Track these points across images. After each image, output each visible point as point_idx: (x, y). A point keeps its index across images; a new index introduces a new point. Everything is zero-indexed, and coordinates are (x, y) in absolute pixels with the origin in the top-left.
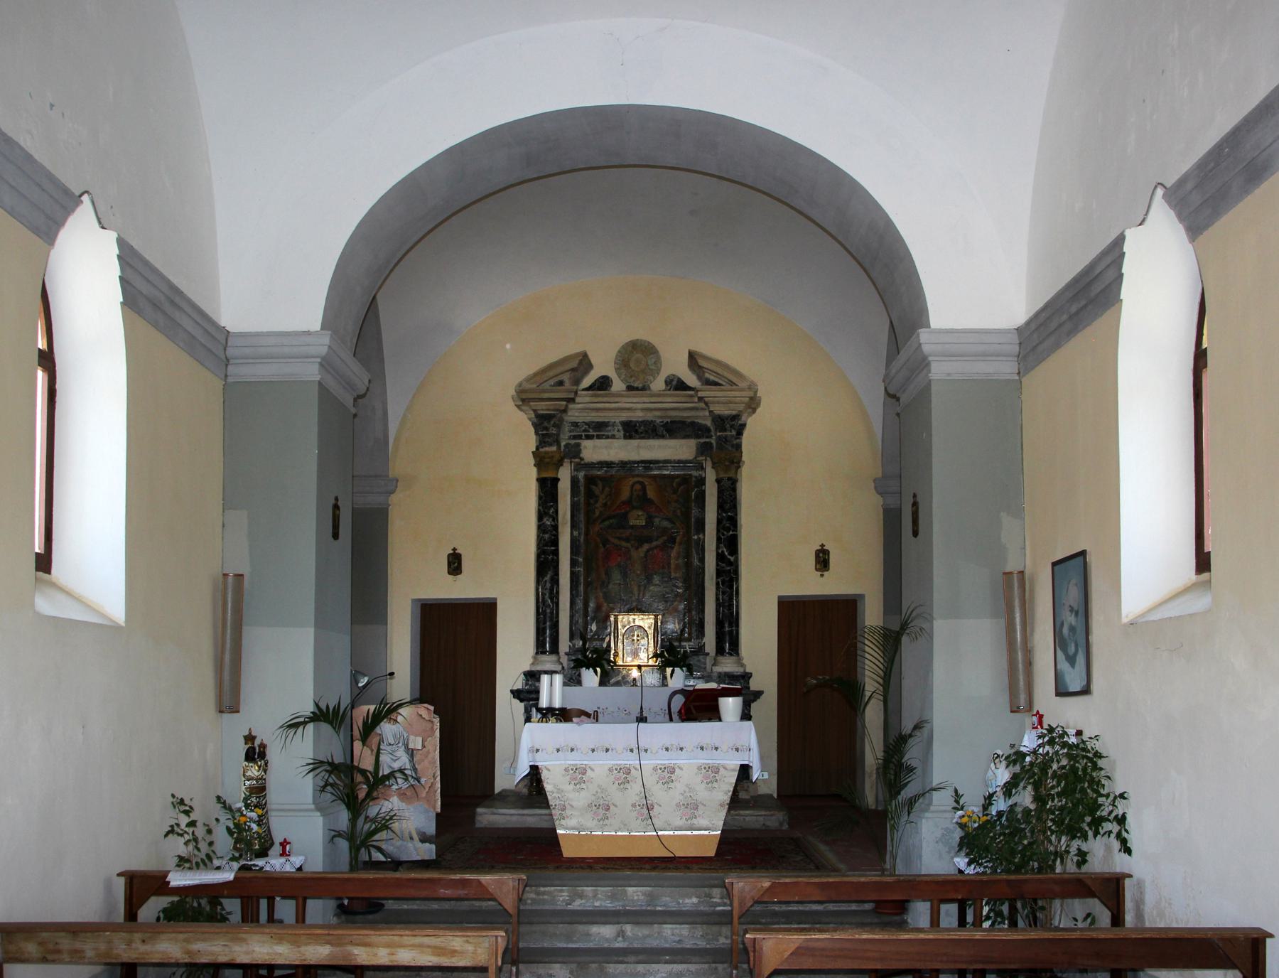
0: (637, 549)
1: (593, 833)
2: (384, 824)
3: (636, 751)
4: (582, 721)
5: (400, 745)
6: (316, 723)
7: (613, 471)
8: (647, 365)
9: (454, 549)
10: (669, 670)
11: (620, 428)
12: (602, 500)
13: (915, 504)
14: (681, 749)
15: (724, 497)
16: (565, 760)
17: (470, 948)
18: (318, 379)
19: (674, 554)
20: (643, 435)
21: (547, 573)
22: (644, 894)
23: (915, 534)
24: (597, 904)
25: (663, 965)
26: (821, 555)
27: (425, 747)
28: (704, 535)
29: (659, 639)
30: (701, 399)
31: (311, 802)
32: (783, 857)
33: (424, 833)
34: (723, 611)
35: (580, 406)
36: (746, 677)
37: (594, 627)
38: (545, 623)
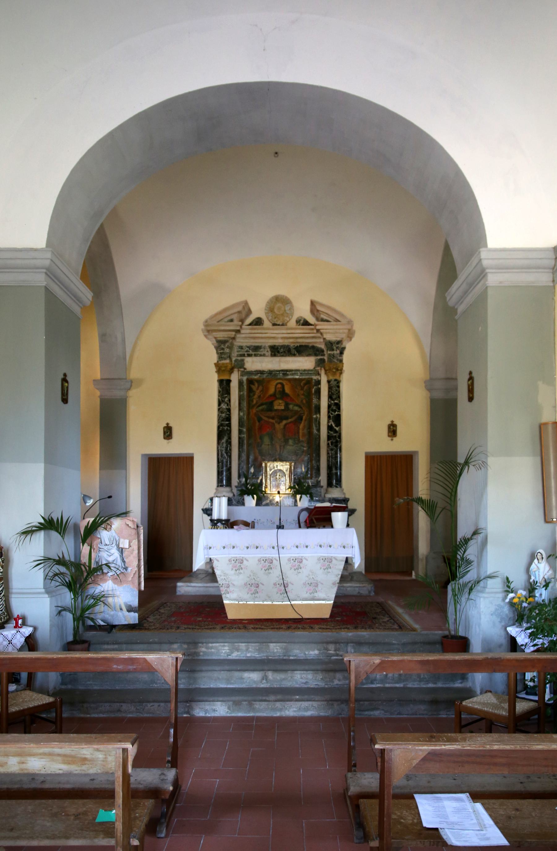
0: (279, 423)
1: (248, 603)
2: (99, 599)
3: (276, 548)
4: (240, 528)
5: (114, 544)
6: (47, 531)
7: (265, 376)
8: (285, 311)
9: (168, 424)
10: (298, 497)
11: (269, 350)
12: (258, 393)
13: (471, 378)
14: (307, 547)
15: (332, 391)
16: (229, 554)
17: (100, 756)
18: (44, 285)
19: (301, 426)
20: (282, 354)
21: (224, 438)
22: (281, 648)
23: (471, 399)
24: (249, 655)
25: (295, 702)
26: (392, 427)
27: (130, 546)
28: (320, 415)
29: (293, 477)
30: (318, 331)
31: (43, 587)
32: (375, 618)
33: (130, 606)
34: (332, 460)
35: (243, 336)
36: (346, 500)
37: (252, 470)
38: (222, 468)
